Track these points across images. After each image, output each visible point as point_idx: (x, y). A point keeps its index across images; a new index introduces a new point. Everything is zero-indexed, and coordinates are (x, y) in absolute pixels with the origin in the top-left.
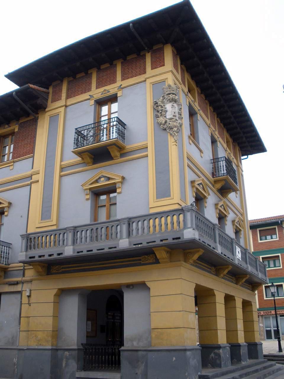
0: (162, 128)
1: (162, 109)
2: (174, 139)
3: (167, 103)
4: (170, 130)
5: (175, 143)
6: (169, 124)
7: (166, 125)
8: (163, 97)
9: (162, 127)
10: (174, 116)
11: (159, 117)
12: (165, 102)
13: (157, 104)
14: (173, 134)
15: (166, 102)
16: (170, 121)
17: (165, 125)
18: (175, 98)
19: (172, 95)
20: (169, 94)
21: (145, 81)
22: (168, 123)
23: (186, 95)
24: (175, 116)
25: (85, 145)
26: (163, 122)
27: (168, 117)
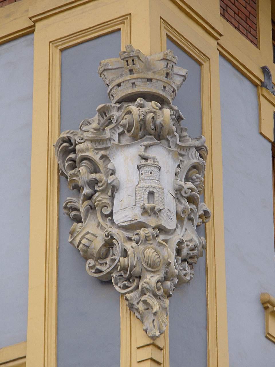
0: (91, 273)
1: (94, 176)
2: (146, 331)
3: (120, 146)
4: (125, 287)
5: (147, 353)
6: (125, 253)
7: (108, 260)
8: (103, 112)
9: (91, 268)
10: (145, 211)
11: (78, 220)
12: (110, 139)
13: (74, 151)
14: (141, 307)
15: (116, 137)
16: (129, 239)
17: (106, 256)
18: (158, 121)
19: (141, 106)
20: (131, 99)
21: (30, 31)
22: (117, 250)
23: (256, 85)
24: (153, 212)
25: (159, 257)
26: (98, 244)
27: (119, 218)
